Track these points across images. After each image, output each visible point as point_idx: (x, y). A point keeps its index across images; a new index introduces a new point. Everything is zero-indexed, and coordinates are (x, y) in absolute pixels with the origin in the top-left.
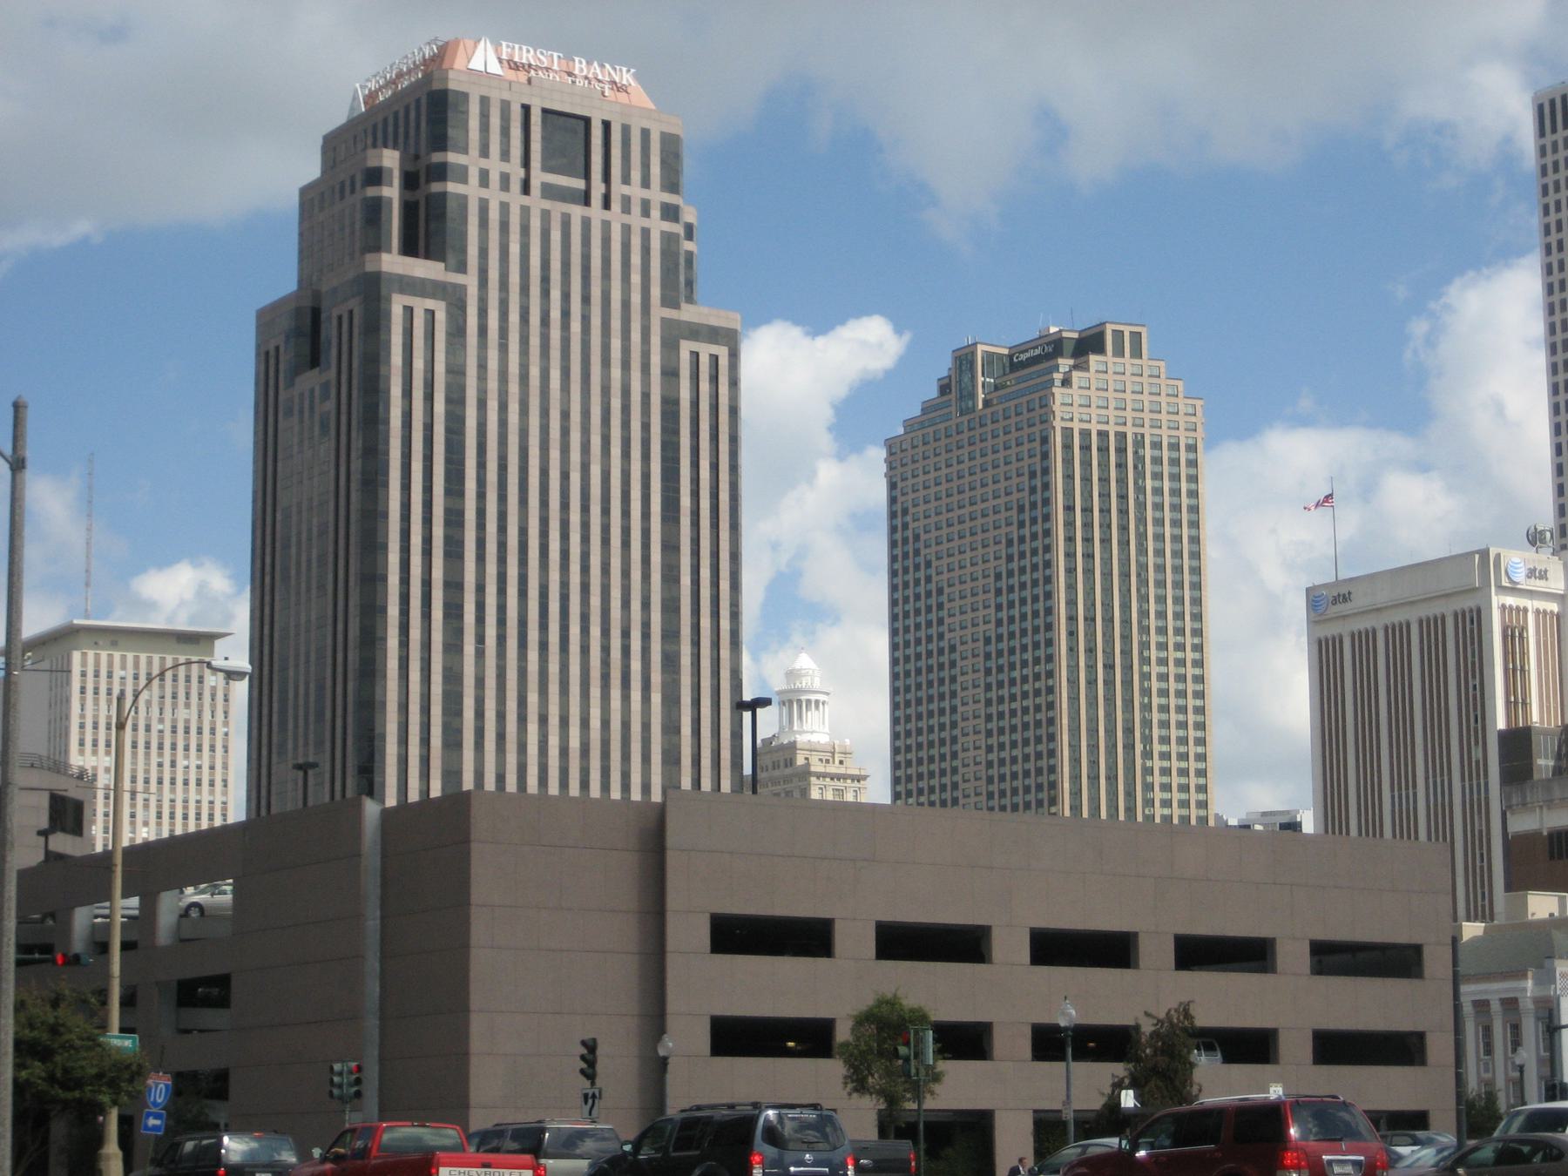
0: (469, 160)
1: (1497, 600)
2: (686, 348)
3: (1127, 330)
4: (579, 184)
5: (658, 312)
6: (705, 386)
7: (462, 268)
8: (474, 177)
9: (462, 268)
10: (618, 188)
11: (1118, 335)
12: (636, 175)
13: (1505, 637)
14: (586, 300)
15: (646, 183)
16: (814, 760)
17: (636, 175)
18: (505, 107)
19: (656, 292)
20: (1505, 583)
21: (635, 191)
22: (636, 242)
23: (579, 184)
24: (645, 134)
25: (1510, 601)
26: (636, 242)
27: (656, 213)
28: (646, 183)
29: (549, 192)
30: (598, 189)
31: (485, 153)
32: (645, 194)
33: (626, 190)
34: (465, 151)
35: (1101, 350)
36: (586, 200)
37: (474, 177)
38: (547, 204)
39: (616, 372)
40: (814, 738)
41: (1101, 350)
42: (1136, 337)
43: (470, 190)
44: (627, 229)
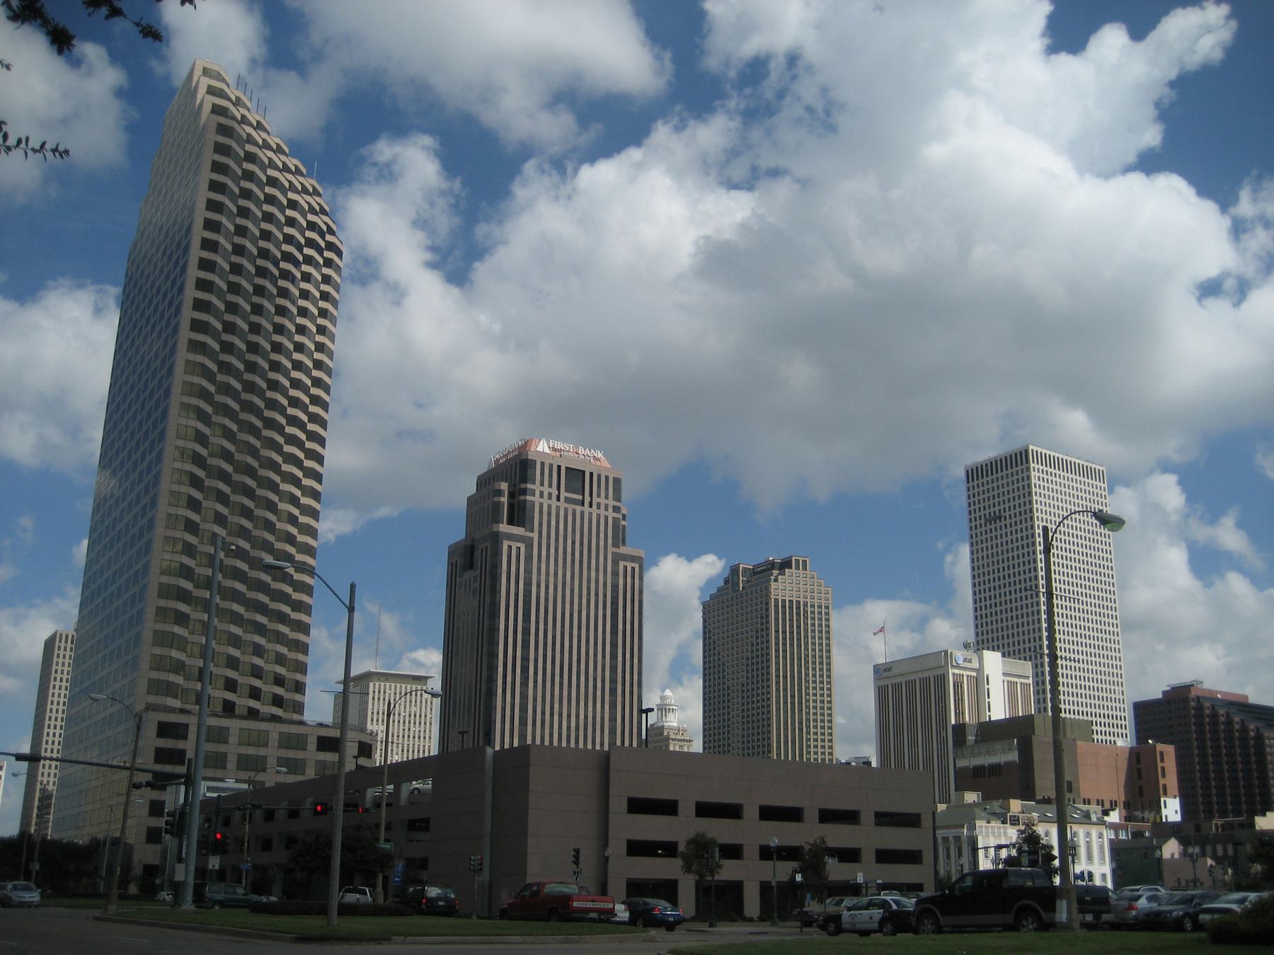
0: (536, 487)
2: (622, 564)
5: (611, 549)
6: (629, 580)
8: (537, 493)
11: (797, 561)
12: (603, 494)
15: (607, 498)
17: (603, 494)
18: (551, 466)
21: (602, 500)
22: (602, 521)
25: (957, 671)
26: (602, 521)
28: (607, 498)
29: (568, 500)
44: (598, 516)
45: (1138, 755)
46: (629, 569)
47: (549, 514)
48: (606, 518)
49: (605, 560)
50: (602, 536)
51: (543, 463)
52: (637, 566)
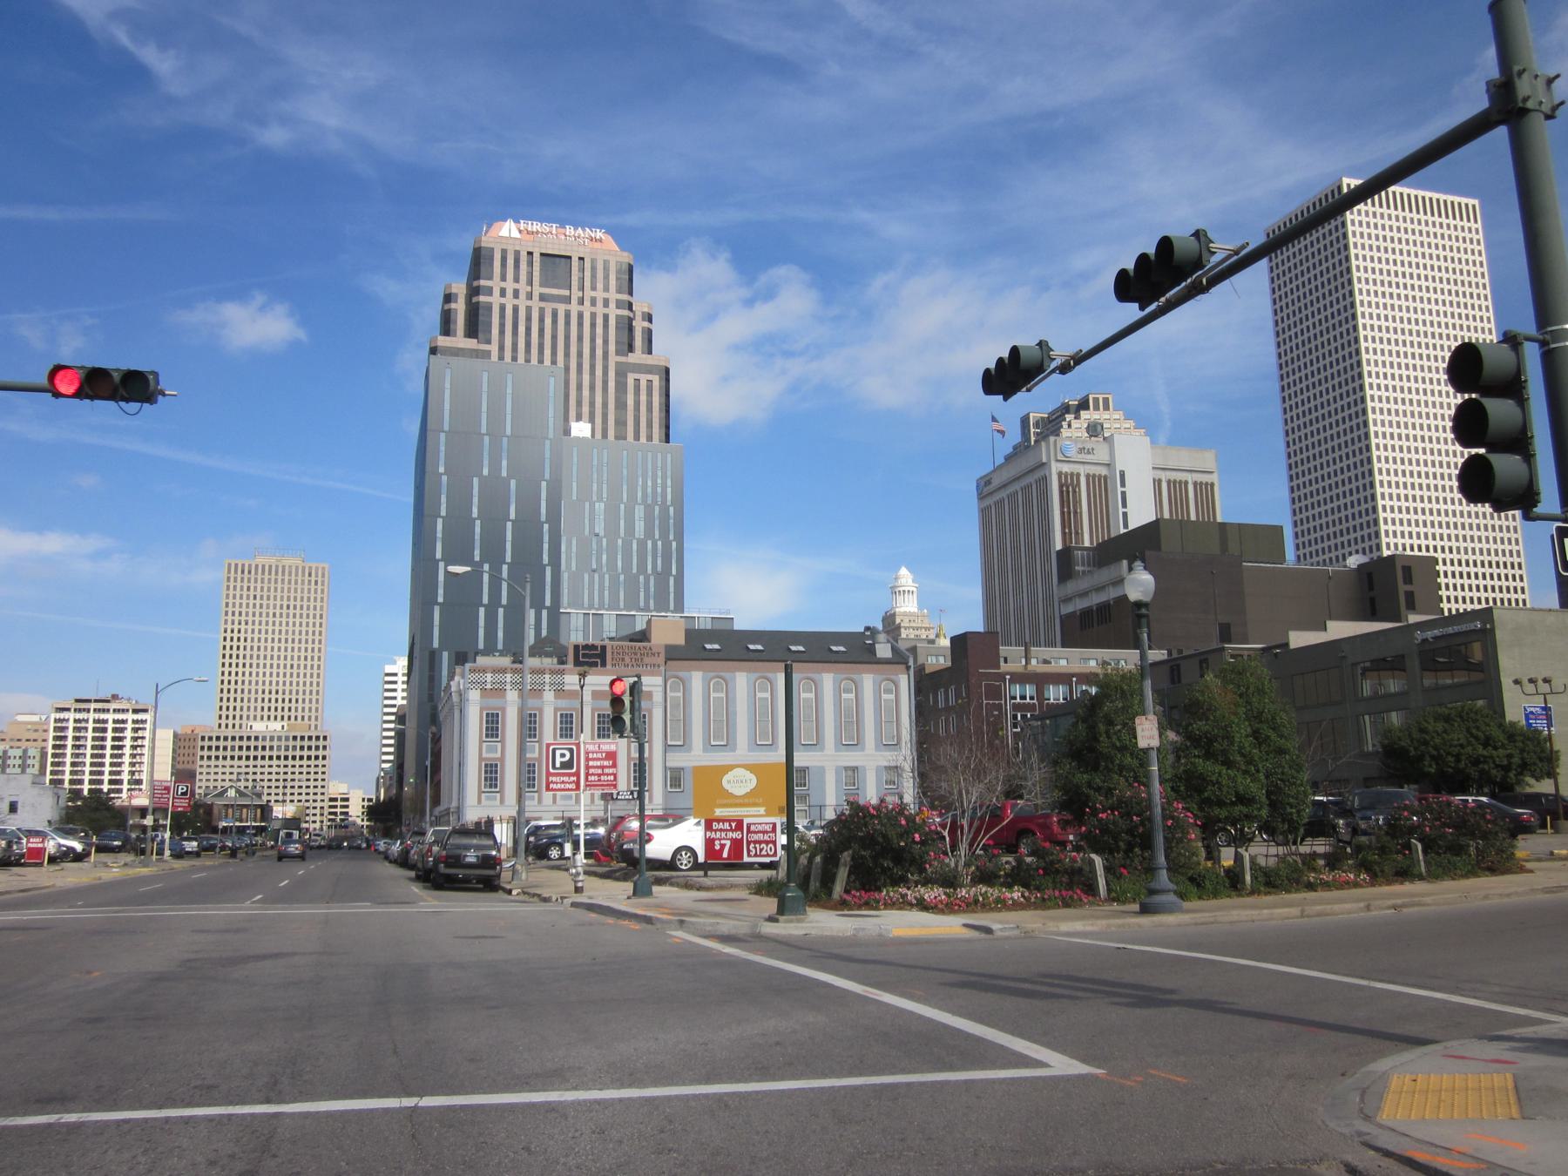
0: (495, 283)
1: (1055, 468)
2: (631, 378)
3: (1101, 397)
4: (566, 293)
5: (613, 359)
6: (643, 398)
7: (489, 342)
8: (497, 292)
9: (489, 342)
10: (589, 293)
11: (1096, 400)
12: (600, 286)
13: (1061, 492)
14: (580, 355)
15: (606, 289)
16: (906, 620)
17: (600, 286)
18: (517, 253)
19: (612, 347)
20: (1060, 457)
21: (600, 295)
22: (600, 321)
23: (566, 293)
24: (606, 263)
25: (1066, 468)
26: (600, 321)
27: (612, 305)
28: (606, 289)
29: (543, 298)
30: (576, 294)
31: (503, 278)
32: (606, 295)
33: (593, 294)
34: (491, 278)
35: (1087, 408)
36: (568, 300)
37: (497, 292)
38: (543, 304)
39: (586, 393)
40: (907, 610)
41: (1087, 408)
42: (1106, 401)
43: (495, 300)
44: (593, 315)
45: (1370, 575)
46: (643, 384)
47: (529, 319)
48: (606, 317)
49: (605, 373)
50: (522, 329)
51: (504, 252)
52: (656, 380)
